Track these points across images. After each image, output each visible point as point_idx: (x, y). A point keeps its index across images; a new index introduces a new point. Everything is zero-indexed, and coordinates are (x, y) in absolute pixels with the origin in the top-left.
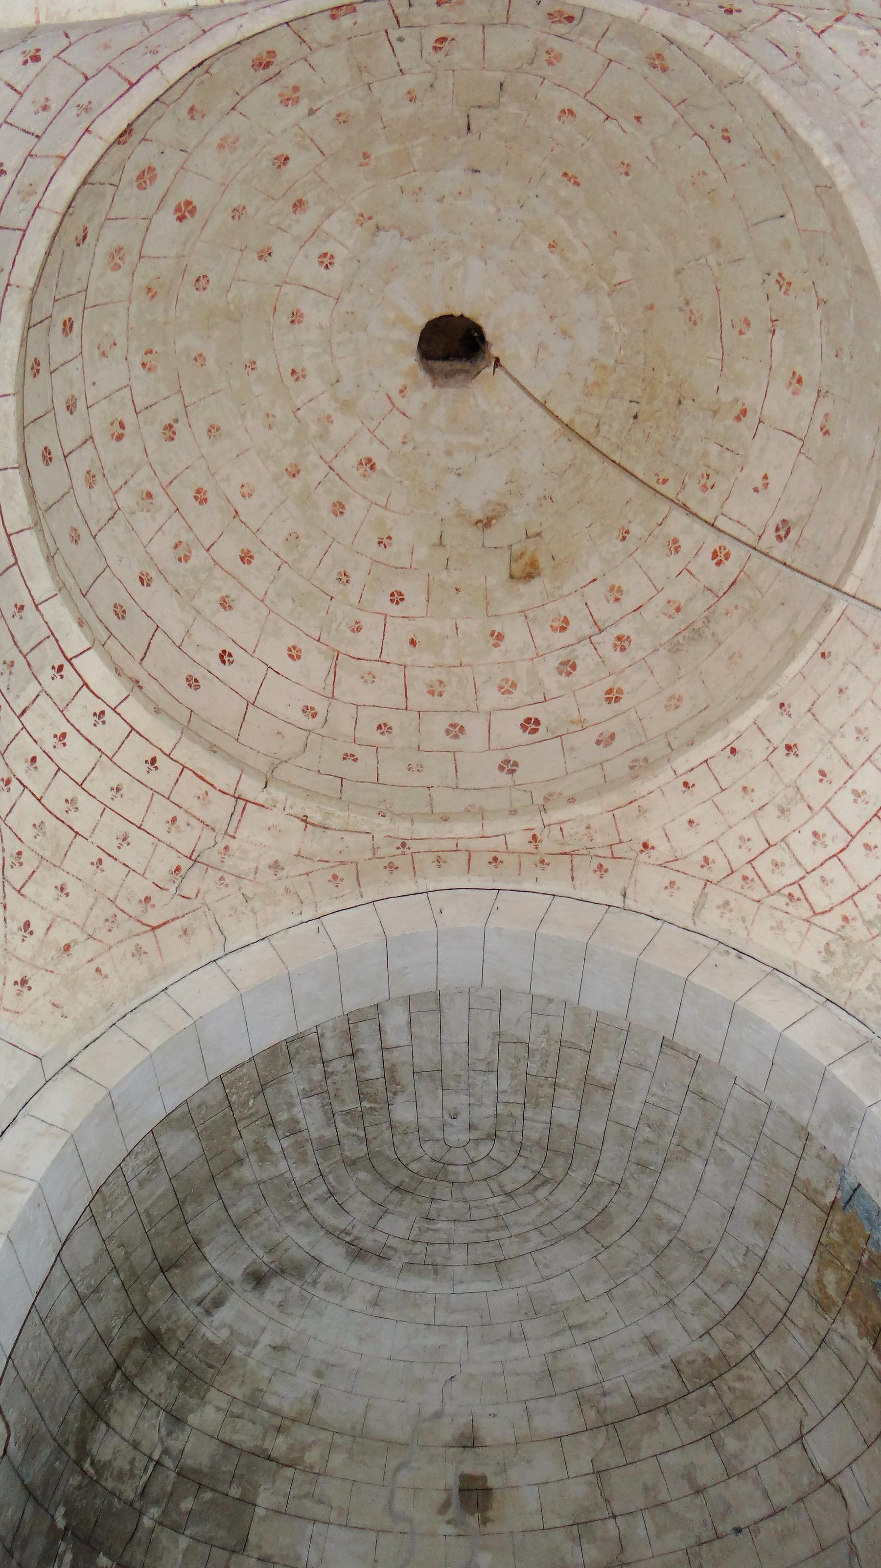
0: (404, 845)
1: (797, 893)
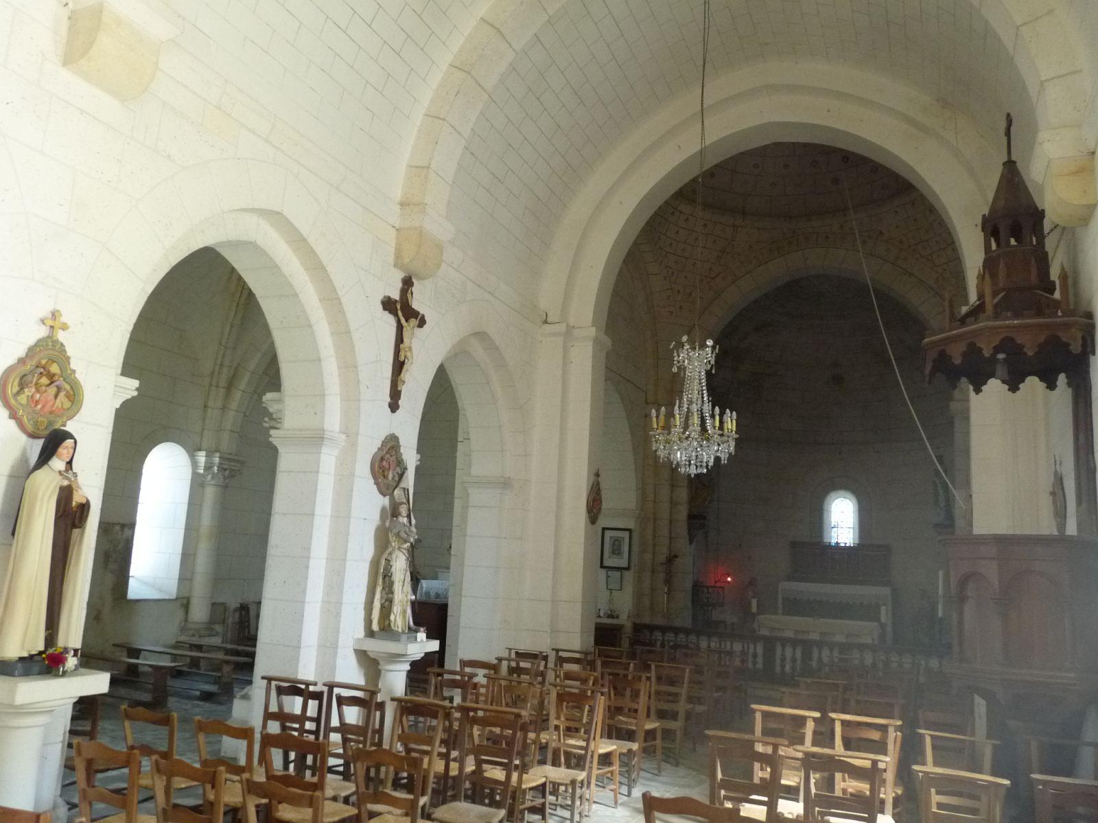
0: (794, 232)
1: (930, 258)
